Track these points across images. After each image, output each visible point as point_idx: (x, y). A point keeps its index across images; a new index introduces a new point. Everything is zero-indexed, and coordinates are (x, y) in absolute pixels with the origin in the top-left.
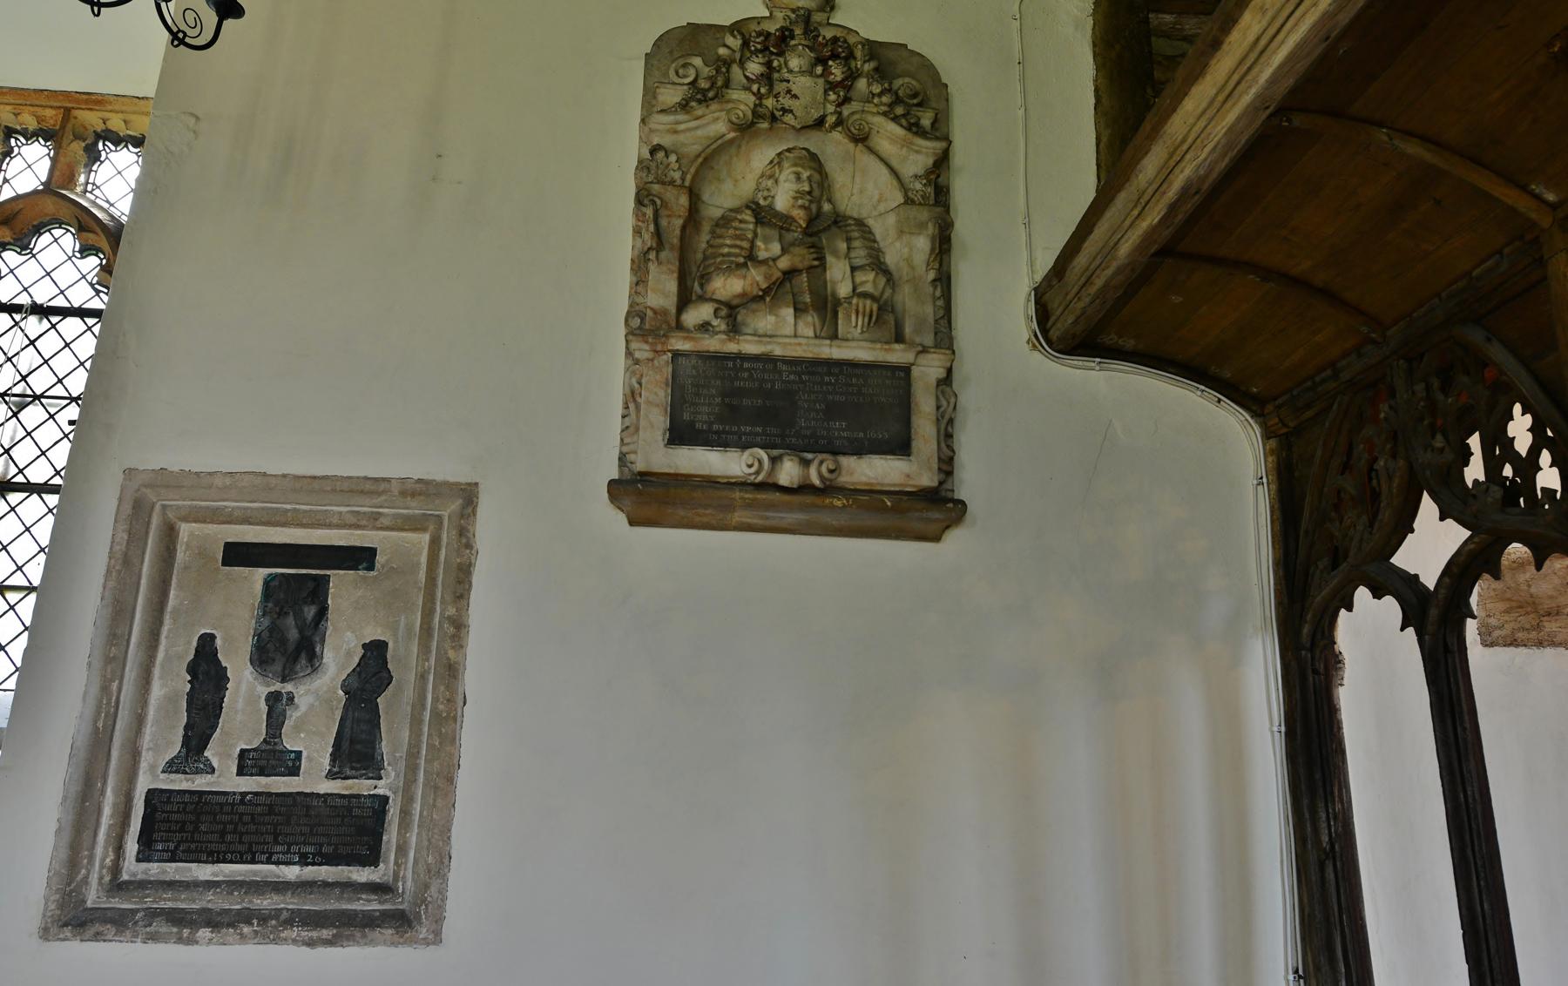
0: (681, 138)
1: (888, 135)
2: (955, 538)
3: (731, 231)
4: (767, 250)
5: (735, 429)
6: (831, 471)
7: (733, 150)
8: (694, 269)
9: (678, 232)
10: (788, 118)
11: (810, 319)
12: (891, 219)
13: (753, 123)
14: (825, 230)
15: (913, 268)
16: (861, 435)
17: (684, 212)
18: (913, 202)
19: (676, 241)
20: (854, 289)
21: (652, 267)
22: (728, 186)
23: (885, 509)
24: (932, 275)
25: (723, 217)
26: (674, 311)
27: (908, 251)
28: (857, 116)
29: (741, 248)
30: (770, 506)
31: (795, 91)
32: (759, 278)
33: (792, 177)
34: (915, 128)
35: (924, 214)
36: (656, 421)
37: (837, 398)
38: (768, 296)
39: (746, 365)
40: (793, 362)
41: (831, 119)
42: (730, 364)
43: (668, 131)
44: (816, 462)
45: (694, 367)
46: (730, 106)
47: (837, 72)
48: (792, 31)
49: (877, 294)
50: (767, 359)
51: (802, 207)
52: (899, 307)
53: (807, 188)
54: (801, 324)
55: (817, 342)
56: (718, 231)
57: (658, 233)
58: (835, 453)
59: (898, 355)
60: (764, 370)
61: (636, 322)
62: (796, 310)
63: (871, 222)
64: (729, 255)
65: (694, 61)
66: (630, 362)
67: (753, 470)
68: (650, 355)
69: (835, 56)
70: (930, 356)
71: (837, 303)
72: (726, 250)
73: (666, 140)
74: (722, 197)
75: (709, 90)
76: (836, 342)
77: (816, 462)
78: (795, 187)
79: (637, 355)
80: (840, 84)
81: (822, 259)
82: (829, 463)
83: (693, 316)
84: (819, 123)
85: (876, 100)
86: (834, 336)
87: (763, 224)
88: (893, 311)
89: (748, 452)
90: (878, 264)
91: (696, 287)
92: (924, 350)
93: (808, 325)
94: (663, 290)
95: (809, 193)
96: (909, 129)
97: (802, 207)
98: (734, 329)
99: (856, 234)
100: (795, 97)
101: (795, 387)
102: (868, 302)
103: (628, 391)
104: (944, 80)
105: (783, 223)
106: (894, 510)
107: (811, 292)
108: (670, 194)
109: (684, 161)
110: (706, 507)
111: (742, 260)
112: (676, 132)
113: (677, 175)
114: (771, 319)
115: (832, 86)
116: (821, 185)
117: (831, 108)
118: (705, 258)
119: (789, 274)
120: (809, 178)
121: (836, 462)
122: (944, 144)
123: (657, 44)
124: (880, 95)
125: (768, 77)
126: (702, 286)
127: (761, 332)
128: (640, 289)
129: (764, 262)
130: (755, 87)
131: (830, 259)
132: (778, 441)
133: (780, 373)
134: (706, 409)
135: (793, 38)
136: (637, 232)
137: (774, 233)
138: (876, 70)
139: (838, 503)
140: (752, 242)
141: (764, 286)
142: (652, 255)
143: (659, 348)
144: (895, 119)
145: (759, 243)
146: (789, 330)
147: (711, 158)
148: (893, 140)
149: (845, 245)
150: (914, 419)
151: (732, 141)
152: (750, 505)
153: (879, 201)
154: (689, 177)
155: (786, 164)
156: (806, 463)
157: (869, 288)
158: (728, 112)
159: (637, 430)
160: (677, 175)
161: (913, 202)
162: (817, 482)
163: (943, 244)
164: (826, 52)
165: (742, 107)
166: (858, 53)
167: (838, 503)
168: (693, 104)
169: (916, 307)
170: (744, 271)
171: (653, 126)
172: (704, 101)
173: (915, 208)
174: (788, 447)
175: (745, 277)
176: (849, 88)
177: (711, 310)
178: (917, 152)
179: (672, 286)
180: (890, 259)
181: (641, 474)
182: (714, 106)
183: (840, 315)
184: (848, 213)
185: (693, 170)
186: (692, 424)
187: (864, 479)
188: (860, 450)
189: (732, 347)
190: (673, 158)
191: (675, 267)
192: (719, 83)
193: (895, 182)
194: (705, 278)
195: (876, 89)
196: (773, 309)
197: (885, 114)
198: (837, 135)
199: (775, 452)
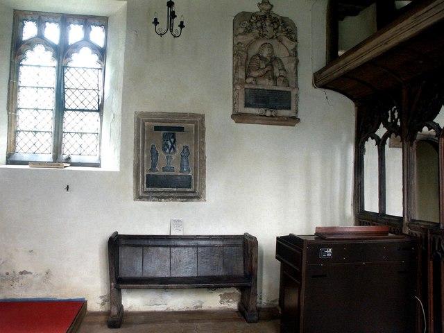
1: (286, 40)
59: (288, 89)
71: (277, 78)
84: (272, 38)
93: (271, 83)
94: (241, 75)
105: (265, 59)
169: (291, 79)
189: (256, 87)
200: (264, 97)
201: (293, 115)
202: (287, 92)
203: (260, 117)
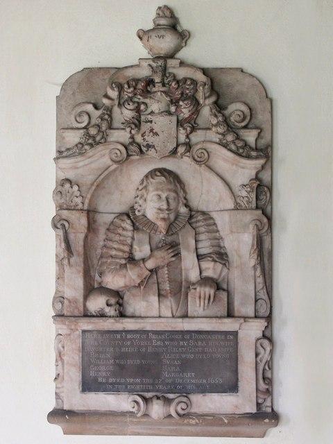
1: (223, 159)
2: (274, 432)
4: (141, 251)
5: (123, 381)
8: (95, 261)
9: (81, 243)
10: (152, 152)
16: (204, 381)
19: (81, 249)
21: (67, 268)
26: (82, 300)
27: (240, 243)
29: (124, 252)
32: (134, 277)
33: (155, 198)
36: (75, 375)
39: (129, 336)
42: (119, 336)
44: (176, 401)
54: (163, 307)
55: (174, 320)
59: (228, 325)
60: (140, 340)
62: (159, 295)
63: (214, 215)
68: (68, 332)
74: (111, 205)
78: (157, 205)
80: (188, 120)
97: (164, 219)
100: (156, 134)
101: (161, 350)
106: (230, 424)
109: (83, 189)
111: (123, 262)
113: (79, 200)
114: (144, 304)
115: (180, 123)
123: (64, 86)
125: (136, 123)
131: (184, 253)
134: (102, 368)
139: (193, 422)
140: (131, 246)
143: (73, 327)
144: (225, 146)
145: (135, 247)
147: (101, 184)
148: (225, 160)
150: (240, 367)
151: (115, 170)
154: (87, 201)
155: (151, 188)
169: (243, 284)
170: (124, 271)
177: (104, 302)
178: (243, 168)
179: (79, 282)
182: (100, 147)
183: (189, 299)
185: (89, 196)
186: (95, 379)
188: (203, 390)
191: (81, 268)
192: (104, 129)
196: (144, 297)
202: (226, 333)
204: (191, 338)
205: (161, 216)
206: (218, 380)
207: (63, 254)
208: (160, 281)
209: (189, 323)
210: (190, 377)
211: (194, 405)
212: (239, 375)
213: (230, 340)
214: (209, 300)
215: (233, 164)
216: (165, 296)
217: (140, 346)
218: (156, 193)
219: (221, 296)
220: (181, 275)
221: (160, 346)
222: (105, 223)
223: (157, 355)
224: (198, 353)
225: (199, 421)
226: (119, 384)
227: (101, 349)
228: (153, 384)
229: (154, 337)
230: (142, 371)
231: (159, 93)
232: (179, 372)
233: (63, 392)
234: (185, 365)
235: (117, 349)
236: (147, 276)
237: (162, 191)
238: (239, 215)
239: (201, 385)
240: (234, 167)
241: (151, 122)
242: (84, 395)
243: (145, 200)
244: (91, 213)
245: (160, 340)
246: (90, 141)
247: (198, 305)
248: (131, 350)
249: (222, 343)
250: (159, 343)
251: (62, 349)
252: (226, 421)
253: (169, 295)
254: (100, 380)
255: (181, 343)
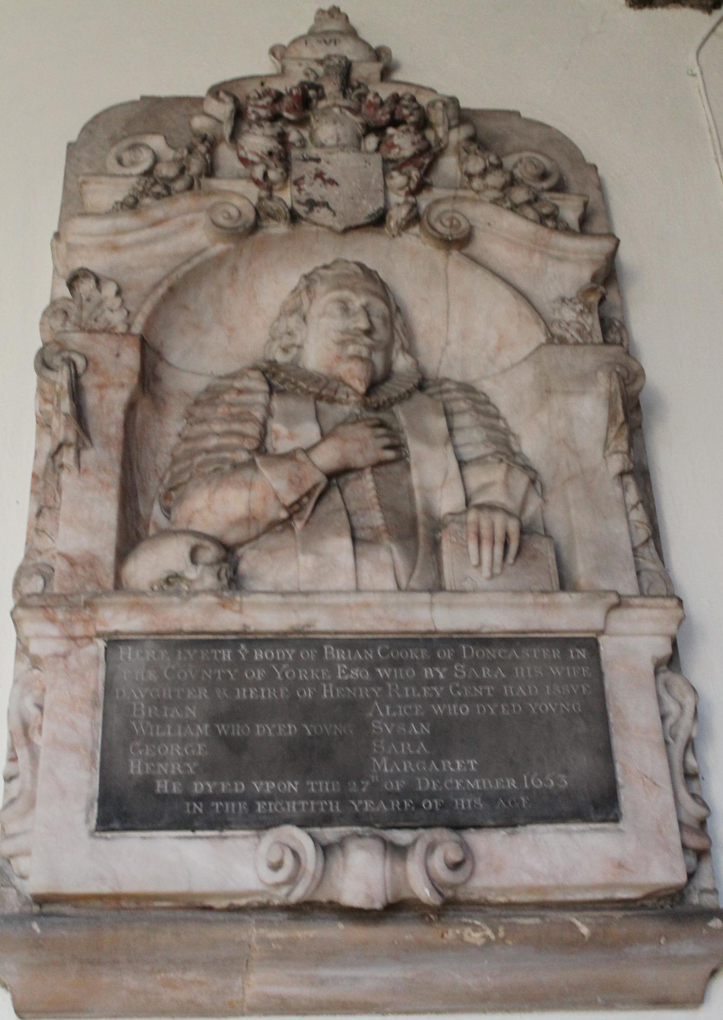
0: (126, 257)
1: (503, 233)
3: (221, 410)
4: (292, 436)
5: (240, 787)
6: (455, 866)
7: (223, 275)
9: (119, 414)
10: (321, 215)
11: (384, 556)
12: (526, 376)
13: (255, 227)
14: (401, 399)
15: (577, 454)
17: (130, 380)
18: (563, 341)
19: (115, 430)
20: (467, 501)
22: (217, 338)
23: (574, 944)
24: (616, 464)
25: (207, 390)
26: (109, 557)
28: (442, 207)
29: (242, 435)
30: (325, 955)
31: (330, 172)
33: (335, 309)
34: (550, 219)
35: (588, 359)
37: (453, 709)
38: (301, 514)
39: (258, 655)
40: (355, 644)
41: (398, 214)
42: (226, 655)
43: (102, 247)
44: (420, 848)
45: (150, 665)
46: (214, 199)
47: (403, 143)
48: (318, 88)
49: (512, 506)
50: (302, 641)
51: (358, 357)
52: (559, 530)
53: (363, 324)
54: (366, 566)
55: (403, 598)
56: (198, 412)
57: (79, 415)
58: (457, 827)
59: (568, 616)
60: (297, 663)
61: (37, 584)
62: (354, 540)
63: (487, 386)
64: (219, 449)
65: (158, 150)
66: (25, 665)
67: (282, 875)
69: (395, 123)
70: (633, 614)
71: (437, 525)
72: (213, 442)
73: (98, 263)
75: (173, 180)
76: (439, 597)
77: (420, 848)
79: (35, 648)
81: (398, 446)
82: (447, 846)
83: (146, 567)
84: (379, 221)
85: (477, 183)
86: (437, 587)
87: (282, 392)
88: (547, 535)
89: (270, 837)
90: (506, 450)
91: (157, 513)
92: (621, 603)
93: (383, 567)
94: (90, 516)
95: (369, 332)
96: (542, 220)
97: (358, 357)
98: (233, 580)
99: (463, 405)
100: (332, 182)
102: (499, 519)
103: (17, 723)
104: (590, 158)
105: (321, 391)
106: (599, 942)
107: (383, 508)
108: (102, 348)
109: (131, 296)
110: (186, 964)
111: (243, 456)
112: (115, 248)
113: (117, 319)
114: (307, 561)
115: (389, 165)
116: (389, 321)
117: (397, 198)
118: (175, 461)
119: (337, 476)
120: (366, 309)
121: (465, 847)
122: (605, 245)
123: (89, 129)
124: (484, 173)
125: (282, 156)
126: (167, 511)
127: (287, 587)
128: (46, 522)
129: (289, 456)
130: (258, 172)
131: (415, 448)
132: (335, 808)
133: (331, 666)
134: (175, 750)
135: (321, 97)
136: (44, 424)
137: (306, 407)
138: (473, 139)
139: (476, 937)
140: (264, 426)
141: (290, 498)
142: (68, 457)
143: (79, 630)
144: (515, 208)
145: (276, 426)
146: (344, 580)
147: (178, 289)
149: (442, 423)
150: (617, 742)
151: (219, 260)
152: (281, 955)
153: (499, 348)
155: (320, 288)
156: (399, 852)
157: (496, 495)
158: (211, 210)
159: (32, 803)
160: (117, 319)
161: (563, 341)
162: (425, 893)
163: (631, 411)
164: (383, 116)
165: (236, 201)
166: (437, 116)
167: (476, 937)
168: (147, 201)
169: (594, 526)
170: (248, 474)
171: (71, 239)
172: (167, 191)
173: (568, 350)
174: (359, 819)
175: (250, 486)
176: (428, 170)
178: (560, 259)
179: (107, 511)
180: (531, 446)
181: (41, 900)
184: (444, 373)
185: (147, 308)
186: (147, 784)
187: (527, 879)
188: (510, 816)
189: (228, 620)
190: (110, 290)
191: (113, 476)
193: (525, 310)
194: (172, 495)
195: (475, 165)
197: (495, 202)
198: (413, 239)
199: (330, 834)
200: (308, 711)
201: (664, 870)
202: (564, 643)
203: (278, 932)
204: (457, 657)
205: (351, 349)
206: (553, 780)
207: (63, 430)
208: (352, 506)
209: (450, 606)
210: (463, 775)
211: (481, 866)
212: (618, 768)
213: (580, 662)
214: (506, 546)
215: (532, 251)
216: (374, 541)
217: (298, 684)
218: (336, 294)
219: (536, 546)
220: (411, 499)
221: (361, 682)
222: (187, 394)
223: (351, 709)
224: (480, 700)
225: (496, 932)
226: (226, 798)
227: (167, 694)
228: (343, 798)
229: (340, 655)
230: (306, 756)
231: (336, 110)
232: (428, 759)
233: (27, 853)
234: (443, 738)
235: (221, 693)
236: (315, 487)
237: (353, 289)
238: (564, 356)
239: (503, 794)
240: (537, 257)
241: (318, 160)
242: (93, 841)
243: (304, 319)
244: (149, 378)
245: (361, 664)
246: (158, 189)
247: (474, 561)
248: (267, 694)
249: (556, 671)
250: (356, 673)
251: (34, 711)
252: (585, 930)
253: (385, 536)
254: (162, 786)
255: (428, 672)
